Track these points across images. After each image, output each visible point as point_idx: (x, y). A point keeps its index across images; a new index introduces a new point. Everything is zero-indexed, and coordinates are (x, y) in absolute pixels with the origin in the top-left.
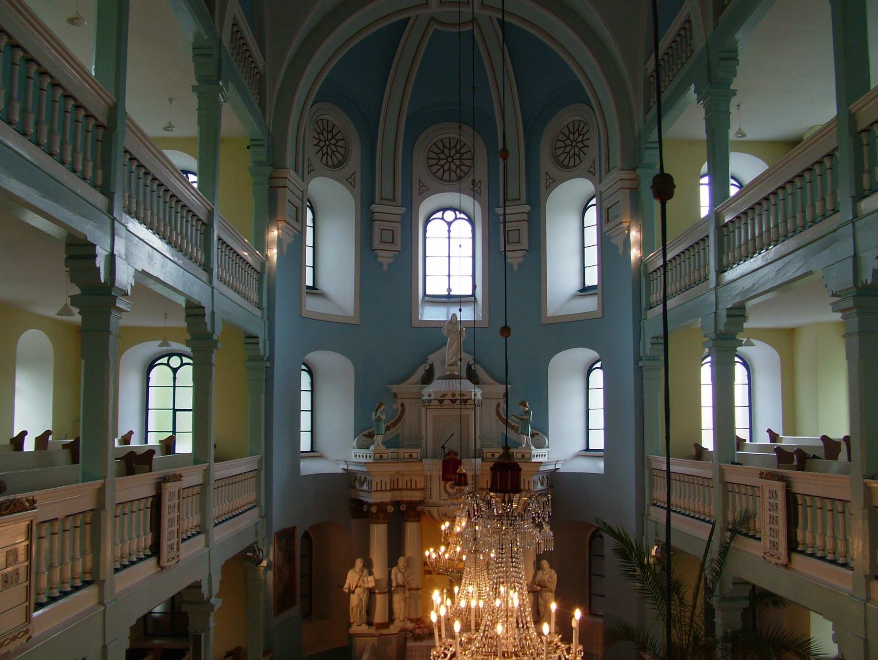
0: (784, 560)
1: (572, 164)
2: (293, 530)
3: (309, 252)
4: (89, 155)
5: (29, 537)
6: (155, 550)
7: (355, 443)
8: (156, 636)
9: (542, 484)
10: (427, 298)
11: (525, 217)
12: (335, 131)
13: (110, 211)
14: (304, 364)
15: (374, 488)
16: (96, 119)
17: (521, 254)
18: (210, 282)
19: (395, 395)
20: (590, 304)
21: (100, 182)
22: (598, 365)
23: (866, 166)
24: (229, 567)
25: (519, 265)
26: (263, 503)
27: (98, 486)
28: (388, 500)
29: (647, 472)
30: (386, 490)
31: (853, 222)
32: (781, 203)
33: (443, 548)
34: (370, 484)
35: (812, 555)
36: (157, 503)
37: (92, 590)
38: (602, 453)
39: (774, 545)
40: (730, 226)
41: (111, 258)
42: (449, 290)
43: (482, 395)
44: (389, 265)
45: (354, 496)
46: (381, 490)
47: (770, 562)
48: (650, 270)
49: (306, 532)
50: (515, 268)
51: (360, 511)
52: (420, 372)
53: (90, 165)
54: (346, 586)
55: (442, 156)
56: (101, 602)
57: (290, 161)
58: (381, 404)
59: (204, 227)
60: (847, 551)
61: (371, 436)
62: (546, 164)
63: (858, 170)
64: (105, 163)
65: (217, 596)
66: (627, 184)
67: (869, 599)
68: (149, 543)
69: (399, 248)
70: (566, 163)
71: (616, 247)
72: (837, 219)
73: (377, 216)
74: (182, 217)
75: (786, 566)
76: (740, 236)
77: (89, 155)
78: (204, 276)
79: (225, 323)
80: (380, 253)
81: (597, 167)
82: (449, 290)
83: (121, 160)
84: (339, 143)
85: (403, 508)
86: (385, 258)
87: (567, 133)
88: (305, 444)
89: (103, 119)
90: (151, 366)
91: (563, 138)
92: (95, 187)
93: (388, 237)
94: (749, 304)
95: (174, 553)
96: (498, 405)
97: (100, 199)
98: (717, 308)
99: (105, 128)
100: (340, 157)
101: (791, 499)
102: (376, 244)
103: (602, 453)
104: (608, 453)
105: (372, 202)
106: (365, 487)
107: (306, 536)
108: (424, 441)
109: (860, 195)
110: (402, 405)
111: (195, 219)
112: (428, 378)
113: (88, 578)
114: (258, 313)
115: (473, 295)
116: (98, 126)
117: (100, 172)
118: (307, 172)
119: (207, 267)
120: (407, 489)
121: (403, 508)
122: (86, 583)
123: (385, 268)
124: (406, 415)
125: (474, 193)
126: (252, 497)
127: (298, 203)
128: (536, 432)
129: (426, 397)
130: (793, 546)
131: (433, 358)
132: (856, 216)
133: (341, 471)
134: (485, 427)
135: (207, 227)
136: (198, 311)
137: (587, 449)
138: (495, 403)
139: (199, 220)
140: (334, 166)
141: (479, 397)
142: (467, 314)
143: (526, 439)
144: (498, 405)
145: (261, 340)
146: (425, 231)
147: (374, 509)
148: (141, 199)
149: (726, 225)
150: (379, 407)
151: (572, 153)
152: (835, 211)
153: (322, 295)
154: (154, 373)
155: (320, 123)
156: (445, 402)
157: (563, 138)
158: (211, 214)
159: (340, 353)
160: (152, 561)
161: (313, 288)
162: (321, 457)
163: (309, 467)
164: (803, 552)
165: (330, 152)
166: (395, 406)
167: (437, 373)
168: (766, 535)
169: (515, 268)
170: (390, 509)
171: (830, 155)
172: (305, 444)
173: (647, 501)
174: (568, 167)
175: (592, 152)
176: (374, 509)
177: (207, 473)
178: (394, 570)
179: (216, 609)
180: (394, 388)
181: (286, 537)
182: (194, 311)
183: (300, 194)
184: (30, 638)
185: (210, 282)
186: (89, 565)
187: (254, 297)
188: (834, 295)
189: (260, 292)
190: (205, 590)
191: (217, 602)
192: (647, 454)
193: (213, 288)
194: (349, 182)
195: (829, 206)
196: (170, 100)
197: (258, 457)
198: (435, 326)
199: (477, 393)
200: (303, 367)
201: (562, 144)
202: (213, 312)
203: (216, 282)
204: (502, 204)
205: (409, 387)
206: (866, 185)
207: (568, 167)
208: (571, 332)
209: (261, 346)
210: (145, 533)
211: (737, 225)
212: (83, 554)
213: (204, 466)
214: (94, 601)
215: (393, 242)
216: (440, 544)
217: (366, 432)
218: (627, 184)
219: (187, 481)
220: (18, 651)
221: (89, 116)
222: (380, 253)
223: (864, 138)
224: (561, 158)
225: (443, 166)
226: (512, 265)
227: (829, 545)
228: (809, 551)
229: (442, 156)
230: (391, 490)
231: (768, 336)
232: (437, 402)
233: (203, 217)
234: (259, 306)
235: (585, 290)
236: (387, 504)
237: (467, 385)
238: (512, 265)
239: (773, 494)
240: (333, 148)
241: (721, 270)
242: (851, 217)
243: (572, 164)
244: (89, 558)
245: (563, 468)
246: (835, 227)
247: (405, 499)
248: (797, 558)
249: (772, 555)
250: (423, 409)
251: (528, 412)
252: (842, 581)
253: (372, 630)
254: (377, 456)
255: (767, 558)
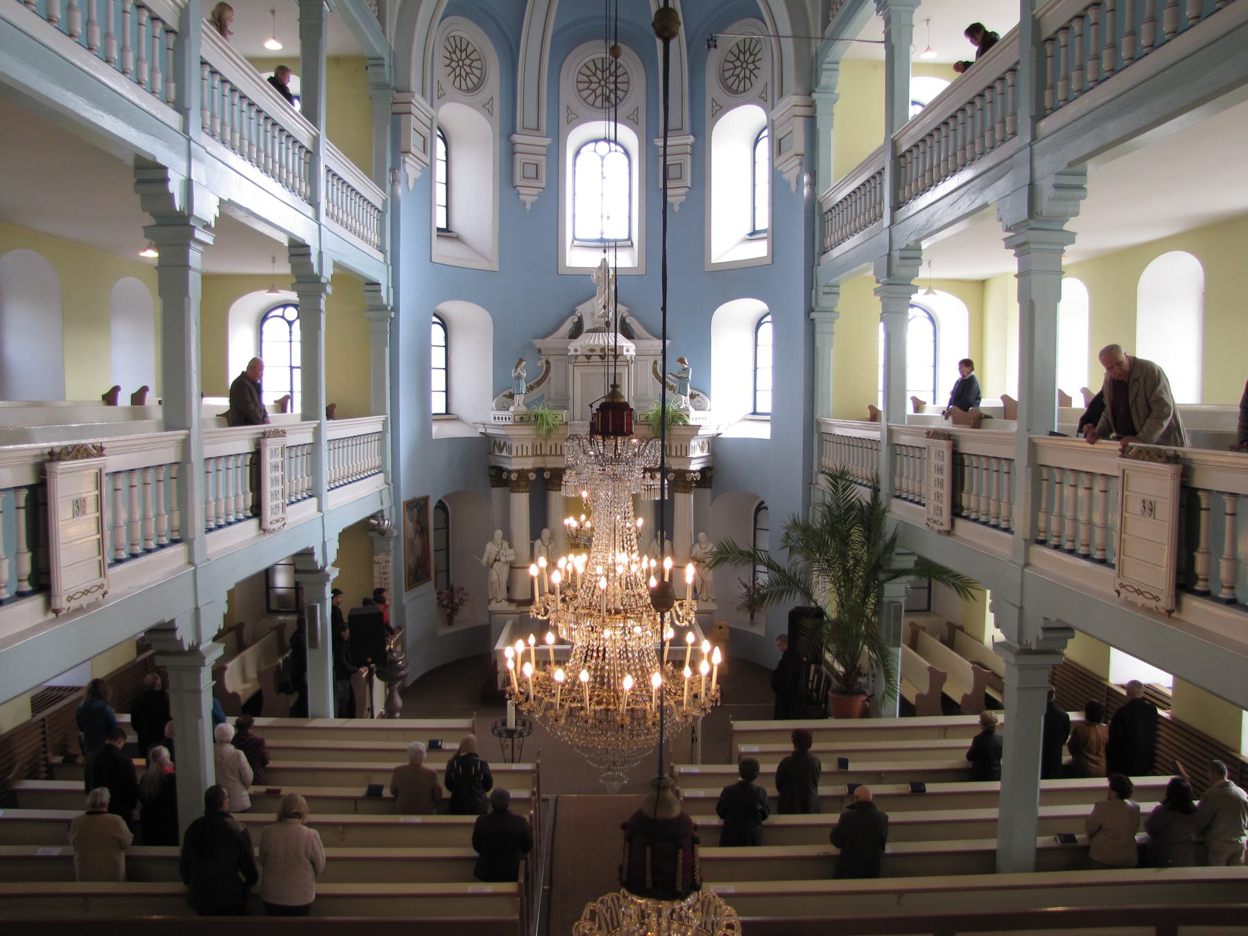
0: (947, 527)
1: (741, 88)
2: (426, 499)
3: (440, 191)
4: (157, 65)
5: (99, 485)
6: (257, 510)
7: (493, 405)
8: (278, 612)
9: (702, 449)
10: (576, 243)
11: (689, 149)
12: (470, 50)
13: (186, 130)
14: (435, 315)
15: (514, 453)
16: (164, 23)
17: (683, 191)
18: (317, 218)
19: (540, 351)
20: (760, 250)
21: (172, 96)
22: (769, 318)
23: (1049, 81)
24: (347, 535)
25: (681, 205)
26: (389, 468)
27: (182, 437)
28: (530, 467)
29: (816, 436)
30: (527, 456)
31: (1031, 145)
32: (960, 127)
33: (583, 517)
34: (510, 452)
35: (975, 520)
36: (256, 460)
37: (180, 549)
38: (768, 417)
39: (939, 510)
40: (908, 156)
41: (189, 183)
42: (602, 233)
43: (636, 351)
44: (532, 204)
45: (493, 464)
46: (522, 456)
47: (933, 528)
48: (825, 210)
49: (440, 502)
50: (677, 208)
51: (499, 477)
52: (568, 325)
53: (159, 77)
54: (486, 555)
55: (594, 79)
56: (191, 562)
57: (415, 84)
58: (521, 361)
59: (308, 156)
60: (1010, 514)
61: (511, 396)
62: (713, 87)
63: (1041, 85)
64: (178, 75)
65: (334, 565)
66: (800, 111)
67: (1027, 564)
68: (250, 503)
69: (543, 185)
70: (734, 87)
71: (788, 184)
72: (1014, 144)
73: (519, 148)
74: (281, 143)
75: (949, 533)
76: (915, 168)
77: (157, 65)
78: (309, 211)
79: (336, 265)
80: (522, 190)
81: (770, 95)
82: (602, 233)
83: (194, 73)
84: (474, 64)
85: (547, 475)
86: (529, 195)
87: (736, 52)
88: (438, 405)
89: (173, 23)
90: (264, 318)
91: (732, 58)
92: (167, 102)
93: (531, 171)
94: (925, 245)
95: (280, 515)
96: (655, 362)
97: (172, 118)
98: (890, 250)
99: (175, 33)
100: (475, 80)
101: (958, 461)
102: (518, 180)
103: (768, 417)
104: (776, 419)
105: (514, 131)
106: (504, 453)
107: (441, 506)
108: (571, 402)
109: (1040, 113)
110: (548, 362)
111: (297, 145)
112: (577, 331)
113: (177, 537)
114: (380, 256)
115: (630, 239)
116: (169, 31)
117: (172, 86)
118: (437, 96)
119: (313, 202)
120: (551, 455)
121: (547, 475)
122: (174, 542)
123: (528, 207)
124: (551, 374)
125: (632, 122)
126: (376, 461)
127: (426, 131)
128: (695, 392)
129: (572, 353)
130: (957, 510)
131: (583, 309)
132: (1034, 138)
133: (478, 435)
134: (639, 390)
135: (312, 155)
136: (302, 251)
137: (755, 413)
138: (652, 360)
139: (301, 147)
140: (468, 90)
141: (632, 352)
142: (626, 260)
143: (685, 401)
144: (655, 362)
145: (386, 62)
146: (574, 165)
147: (514, 477)
148: (227, 119)
149: (903, 156)
150: (520, 363)
151: (742, 76)
152: (1014, 134)
153: (457, 238)
154: (268, 325)
155: (452, 40)
156: (593, 358)
157: (732, 58)
158: (316, 140)
159: (472, 301)
160: (254, 523)
161: (447, 230)
162: (457, 419)
163: (440, 431)
164: (966, 518)
165: (463, 74)
166: (539, 364)
167: (587, 325)
168: (932, 503)
169: (677, 208)
170: (532, 476)
171: (1013, 70)
172: (438, 405)
173: (815, 468)
174: (737, 88)
175: (765, 73)
176: (514, 477)
177: (317, 432)
178: (538, 543)
179: (332, 578)
180: (539, 343)
181: (417, 506)
182: (298, 250)
183: (428, 122)
184: (105, 593)
185: (317, 218)
186: (176, 523)
187: (375, 238)
188: (1008, 230)
189: (381, 234)
190: (318, 557)
191: (334, 573)
192: (819, 415)
193: (320, 225)
194: (486, 109)
195: (1008, 130)
196: (273, 12)
197: (382, 418)
198: (582, 276)
199: (628, 348)
200: (435, 319)
201: (731, 66)
202: (320, 252)
203: (323, 218)
204: (661, 133)
205: (551, 342)
206: (1048, 104)
207: (737, 92)
208: (739, 281)
209: (383, 293)
210: (245, 493)
211: (915, 154)
212: (170, 511)
213: (314, 423)
214: (182, 560)
215: (537, 178)
216: (582, 512)
217: (507, 392)
218: (800, 111)
219: (291, 440)
220: (91, 606)
221: (155, 19)
222: (522, 190)
223: (1049, 48)
224: (730, 82)
225: (594, 91)
226: (672, 205)
227: (993, 510)
228: (973, 516)
229: (594, 79)
230: (533, 456)
231: (955, 286)
232: (584, 359)
233: (307, 144)
234: (381, 249)
235: (754, 234)
236: (529, 471)
237: (623, 341)
238: (672, 205)
239: (939, 455)
240: (468, 69)
241: (897, 205)
242: (1028, 140)
243: (741, 88)
244: (176, 515)
245: (726, 434)
246: (1011, 153)
247: (549, 466)
248: (960, 523)
249: (935, 522)
250: (571, 366)
251: (681, 370)
252: (1001, 546)
253: (513, 607)
254: (517, 418)
255: (931, 524)
